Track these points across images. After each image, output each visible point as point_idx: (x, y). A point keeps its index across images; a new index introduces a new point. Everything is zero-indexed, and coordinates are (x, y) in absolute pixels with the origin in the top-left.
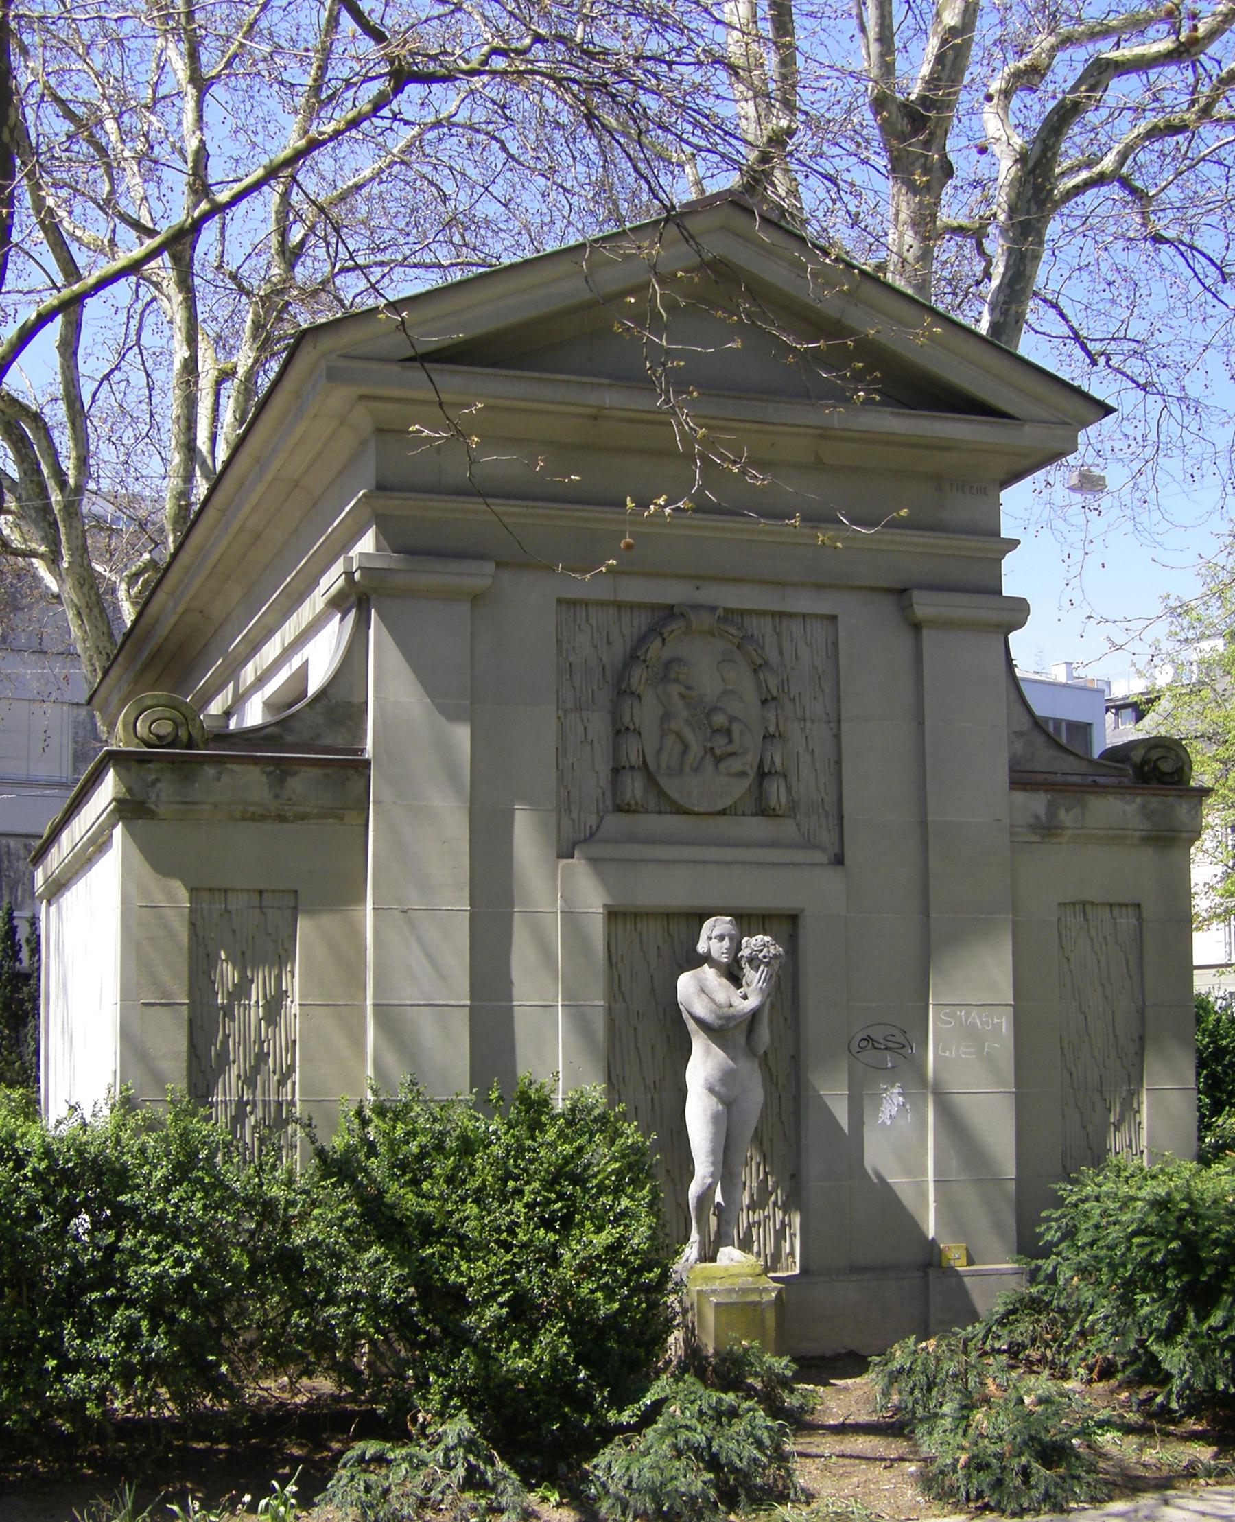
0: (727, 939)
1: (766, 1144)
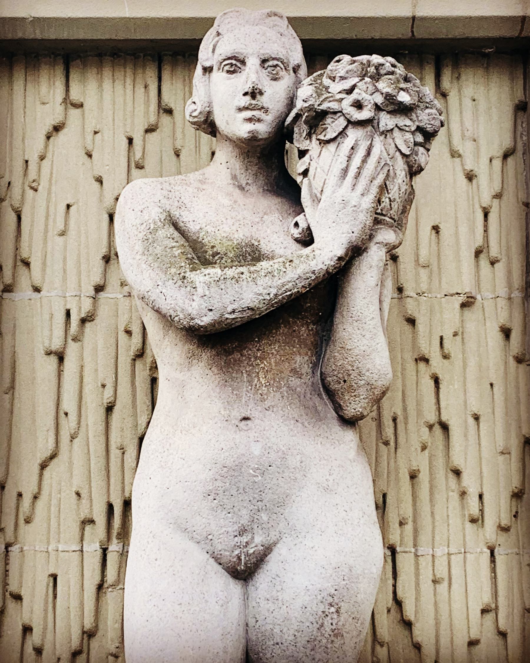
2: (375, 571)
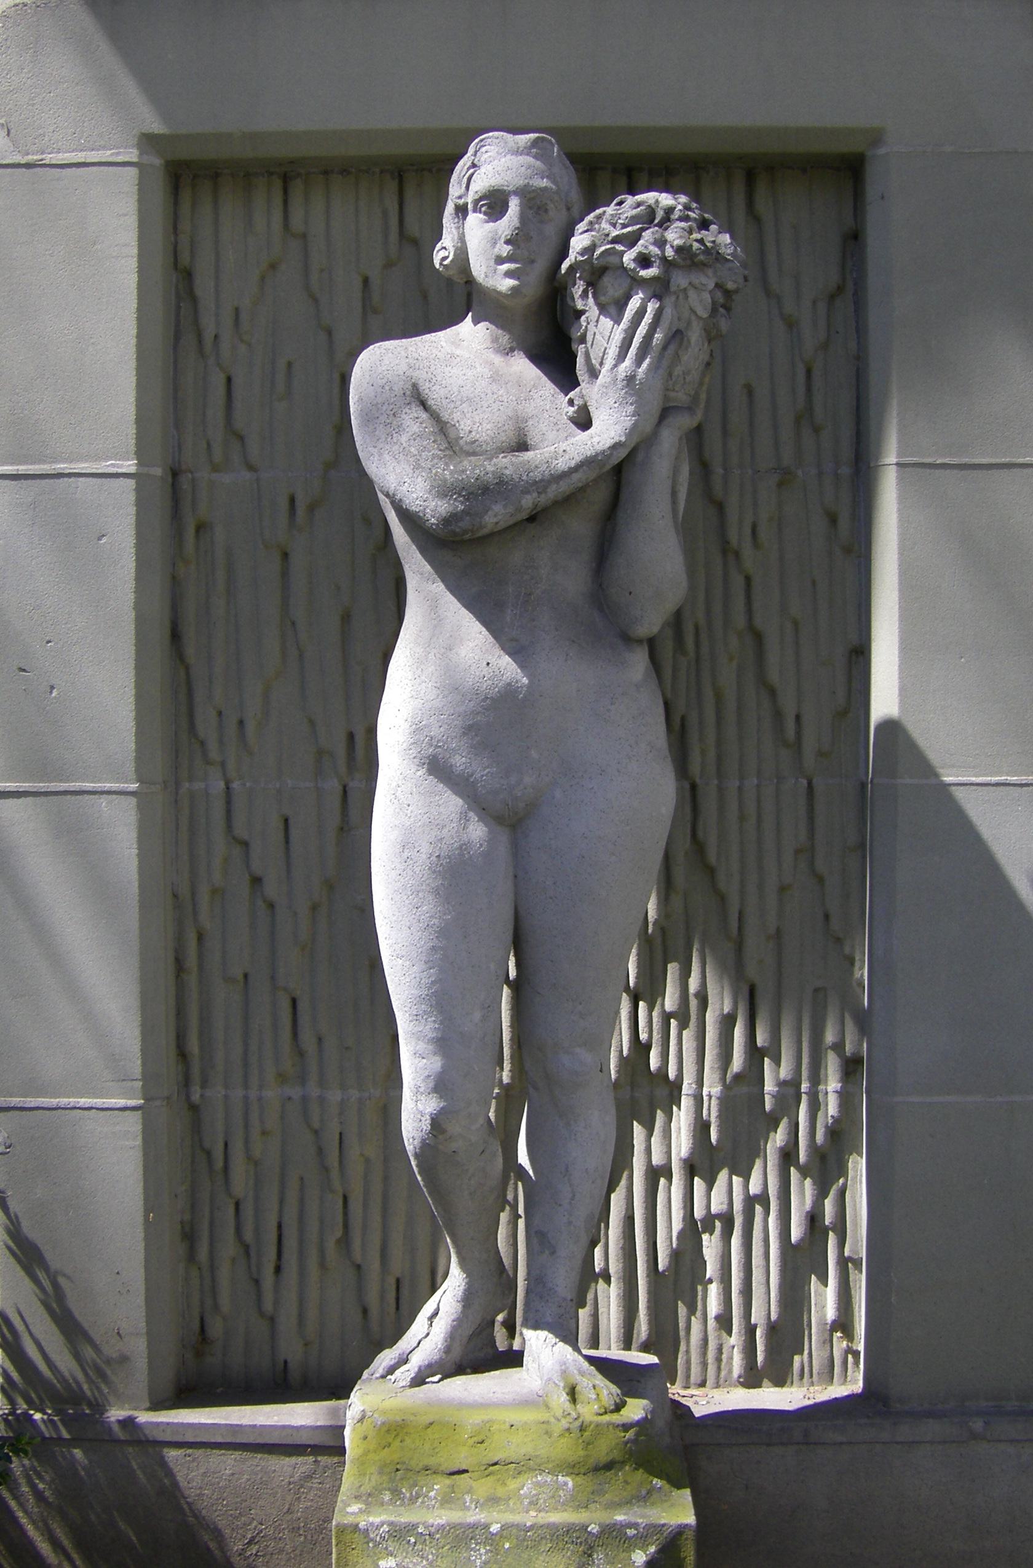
0: (514, 204)
1: (756, 946)
2: (664, 810)
